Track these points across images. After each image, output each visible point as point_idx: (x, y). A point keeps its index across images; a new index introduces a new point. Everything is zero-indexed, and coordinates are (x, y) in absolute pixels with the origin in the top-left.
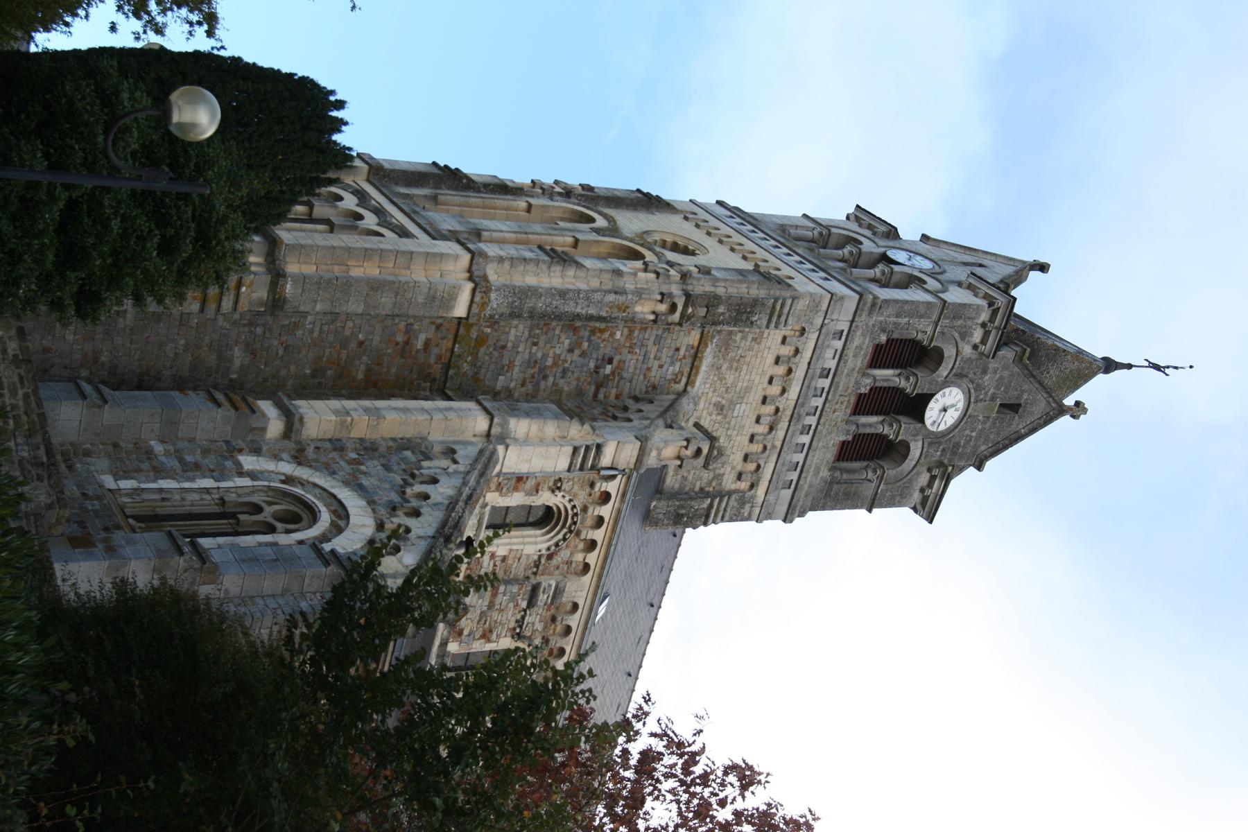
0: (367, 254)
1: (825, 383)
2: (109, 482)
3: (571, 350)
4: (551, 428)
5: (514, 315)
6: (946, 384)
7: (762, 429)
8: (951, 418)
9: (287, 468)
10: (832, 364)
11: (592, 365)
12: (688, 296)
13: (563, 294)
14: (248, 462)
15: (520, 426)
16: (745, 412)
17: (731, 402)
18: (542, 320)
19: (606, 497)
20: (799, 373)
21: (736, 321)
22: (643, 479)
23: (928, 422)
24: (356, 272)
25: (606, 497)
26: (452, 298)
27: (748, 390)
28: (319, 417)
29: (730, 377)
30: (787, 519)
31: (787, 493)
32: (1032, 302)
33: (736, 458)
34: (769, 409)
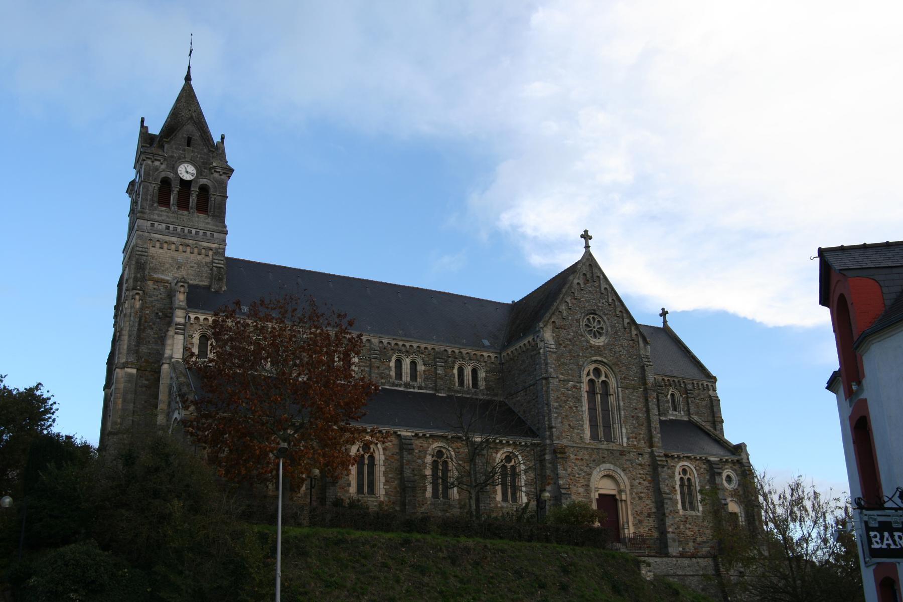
0: (115, 403)
1: (171, 227)
4: (169, 342)
5: (137, 352)
6: (176, 173)
7: (188, 249)
10: (164, 225)
12: (133, 289)
13: (130, 336)
15: (168, 353)
16: (180, 257)
18: (140, 340)
19: (197, 318)
20: (167, 238)
21: (144, 269)
22: (189, 307)
23: (192, 178)
24: (120, 406)
25: (197, 318)
26: (130, 375)
27: (172, 258)
29: (167, 266)
30: (226, 233)
31: (216, 235)
32: (155, 129)
33: (199, 257)
34: (181, 248)
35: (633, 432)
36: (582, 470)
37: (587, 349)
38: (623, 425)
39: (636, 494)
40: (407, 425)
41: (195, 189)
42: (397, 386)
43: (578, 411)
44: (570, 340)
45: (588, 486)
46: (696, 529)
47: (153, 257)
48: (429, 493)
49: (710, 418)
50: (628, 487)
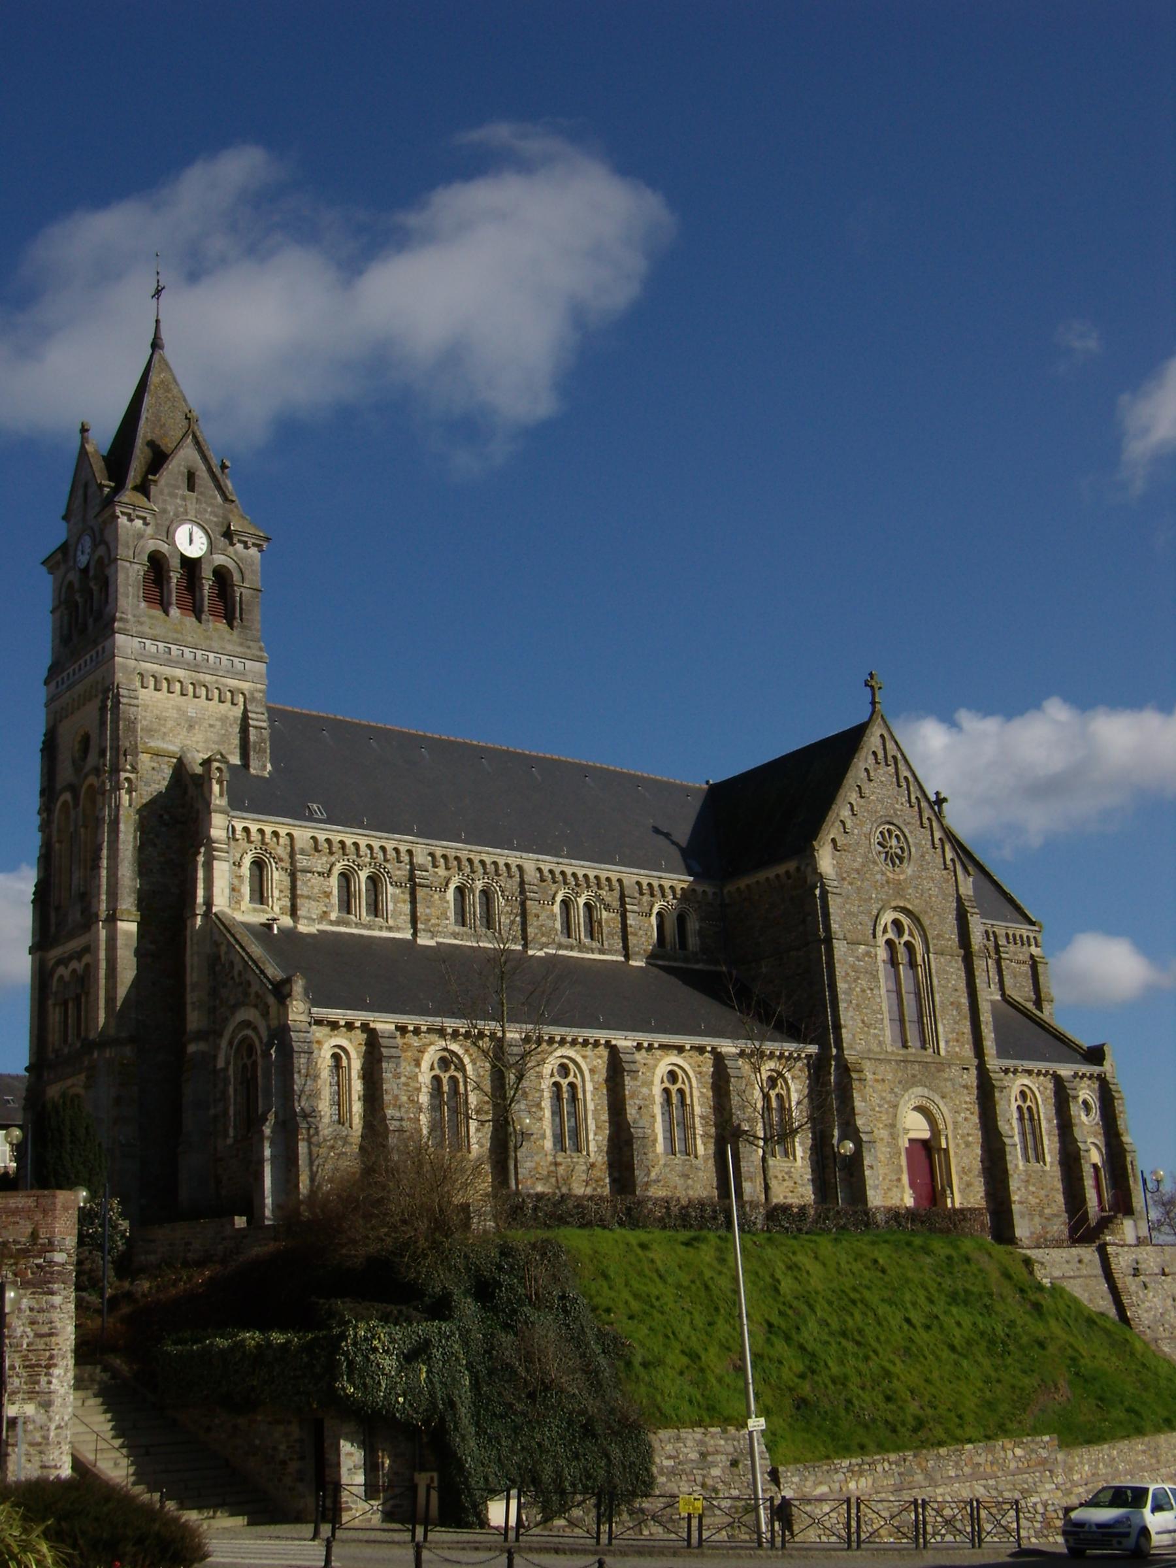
2: (230, 1141)
3: (155, 845)
8: (199, 534)
9: (224, 1043)
11: (164, 829)
14: (221, 1064)
16: (193, 707)
17: (187, 721)
19: (246, 830)
20: (168, 671)
27: (179, 709)
28: (194, 1020)
35: (953, 1031)
36: (883, 1099)
37: (882, 886)
38: (939, 1019)
39: (962, 1137)
40: (734, 1036)
41: (207, 573)
42: (566, 948)
43: (874, 996)
44: (858, 871)
45: (893, 1126)
46: (1043, 1193)
47: (146, 707)
48: (660, 1147)
49: (1034, 997)
50: (950, 1127)
